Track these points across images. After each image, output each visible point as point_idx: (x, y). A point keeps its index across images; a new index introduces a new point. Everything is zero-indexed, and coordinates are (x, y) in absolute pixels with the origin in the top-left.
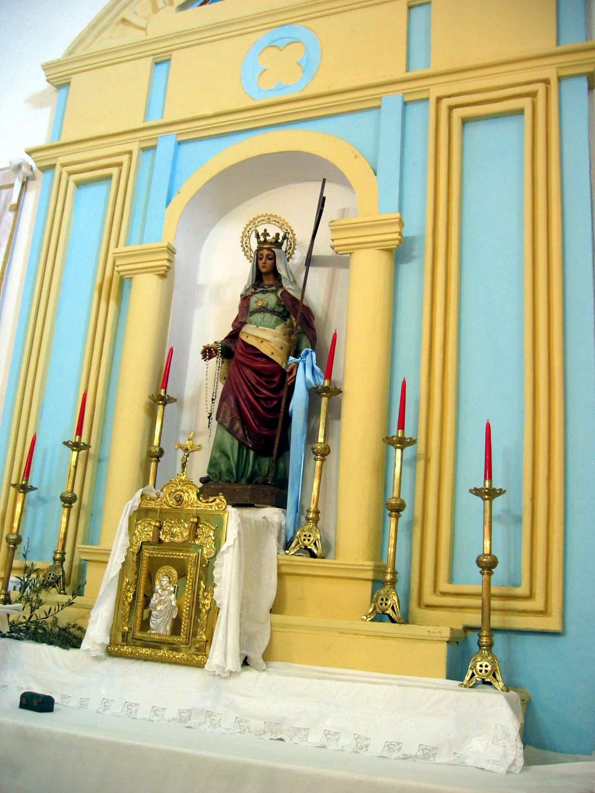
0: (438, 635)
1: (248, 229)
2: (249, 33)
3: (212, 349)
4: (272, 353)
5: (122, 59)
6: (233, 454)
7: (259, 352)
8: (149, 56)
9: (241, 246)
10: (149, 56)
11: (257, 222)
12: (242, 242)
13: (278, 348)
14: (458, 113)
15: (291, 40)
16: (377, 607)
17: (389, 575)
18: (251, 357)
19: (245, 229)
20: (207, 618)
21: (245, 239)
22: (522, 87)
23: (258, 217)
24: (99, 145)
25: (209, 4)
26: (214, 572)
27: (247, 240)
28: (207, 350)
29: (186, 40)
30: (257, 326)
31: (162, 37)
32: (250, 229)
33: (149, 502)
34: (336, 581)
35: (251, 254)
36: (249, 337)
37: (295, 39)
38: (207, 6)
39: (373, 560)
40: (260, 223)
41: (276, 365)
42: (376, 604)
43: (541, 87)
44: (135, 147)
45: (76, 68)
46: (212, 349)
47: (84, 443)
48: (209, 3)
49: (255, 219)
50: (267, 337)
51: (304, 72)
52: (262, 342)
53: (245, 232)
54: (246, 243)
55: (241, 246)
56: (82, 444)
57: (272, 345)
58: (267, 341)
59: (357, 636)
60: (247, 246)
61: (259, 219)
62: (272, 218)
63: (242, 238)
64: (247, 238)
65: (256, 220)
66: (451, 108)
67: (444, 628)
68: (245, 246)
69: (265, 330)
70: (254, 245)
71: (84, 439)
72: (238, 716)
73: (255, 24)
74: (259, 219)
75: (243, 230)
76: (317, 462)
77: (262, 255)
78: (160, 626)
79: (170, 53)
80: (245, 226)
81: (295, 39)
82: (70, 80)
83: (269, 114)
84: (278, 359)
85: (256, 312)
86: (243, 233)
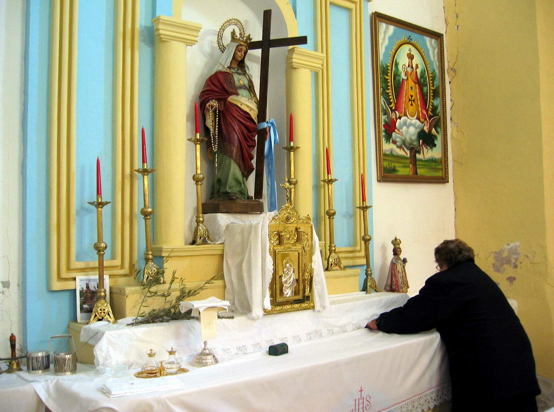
23: (233, 19)
49: (230, 20)
50: (246, 103)
77: (241, 49)
78: (288, 292)
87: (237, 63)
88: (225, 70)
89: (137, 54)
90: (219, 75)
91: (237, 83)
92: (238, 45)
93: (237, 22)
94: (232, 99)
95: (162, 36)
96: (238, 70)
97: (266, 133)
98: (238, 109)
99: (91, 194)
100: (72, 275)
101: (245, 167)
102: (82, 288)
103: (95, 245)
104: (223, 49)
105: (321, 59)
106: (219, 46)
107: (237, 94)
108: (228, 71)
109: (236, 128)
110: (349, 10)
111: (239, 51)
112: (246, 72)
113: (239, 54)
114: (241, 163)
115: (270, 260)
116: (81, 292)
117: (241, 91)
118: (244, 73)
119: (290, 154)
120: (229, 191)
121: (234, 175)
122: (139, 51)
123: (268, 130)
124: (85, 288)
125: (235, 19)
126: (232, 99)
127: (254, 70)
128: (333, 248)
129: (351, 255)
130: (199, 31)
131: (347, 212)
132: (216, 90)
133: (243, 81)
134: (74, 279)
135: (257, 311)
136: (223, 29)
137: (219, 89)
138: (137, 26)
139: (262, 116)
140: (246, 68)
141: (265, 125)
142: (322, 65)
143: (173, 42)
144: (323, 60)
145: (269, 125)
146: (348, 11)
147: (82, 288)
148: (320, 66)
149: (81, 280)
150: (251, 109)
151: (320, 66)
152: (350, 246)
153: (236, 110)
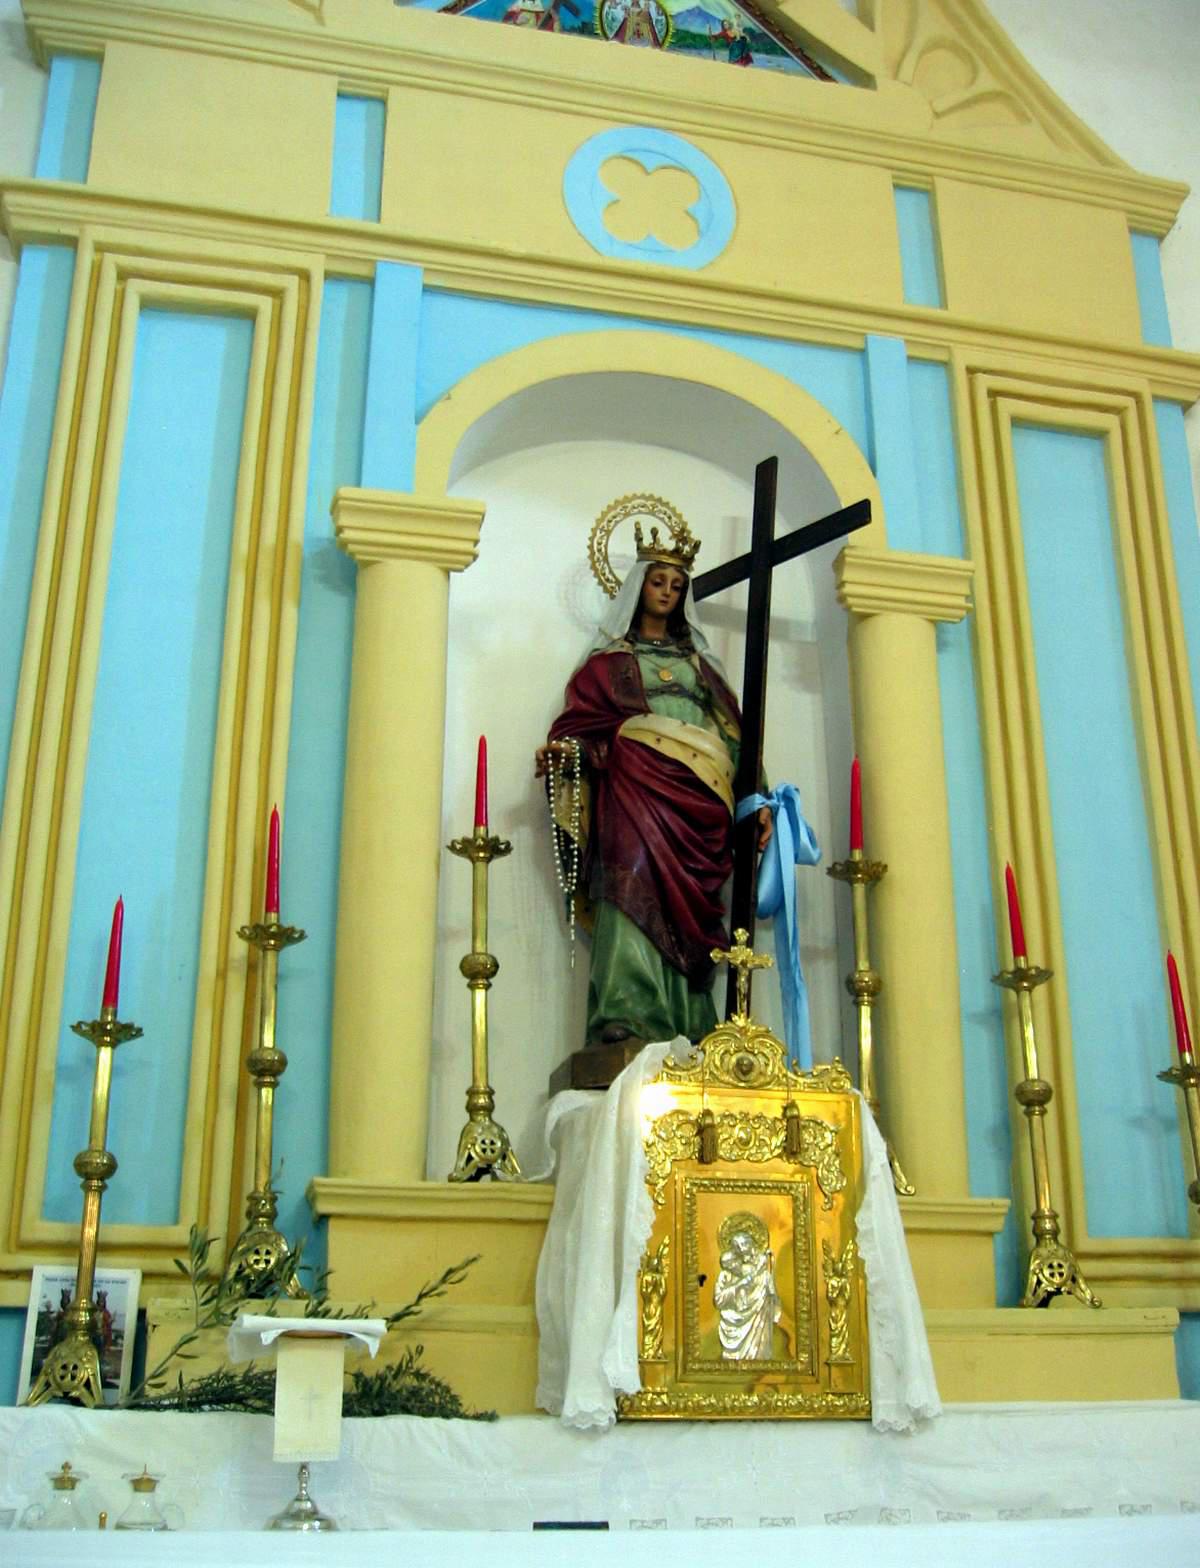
0: (1163, 1322)
1: (609, 516)
2: (539, 107)
3: (564, 755)
4: (716, 782)
5: (543, 102)
6: (658, 981)
7: (691, 775)
8: (333, 73)
9: (589, 547)
10: (333, 73)
11: (630, 505)
12: (591, 539)
13: (724, 775)
14: (136, 288)
15: (667, 162)
16: (1044, 1280)
17: (1047, 1221)
18: (675, 783)
19: (604, 514)
20: (662, 1312)
21: (598, 534)
22: (1075, 391)
23: (635, 497)
24: (214, 231)
25: (462, 15)
26: (856, 1219)
27: (602, 537)
28: (550, 755)
29: (929, 161)
30: (684, 723)
31: (231, 21)
32: (614, 517)
33: (672, 1072)
34: (378, 1225)
35: (603, 568)
36: (662, 742)
37: (676, 161)
38: (458, 19)
39: (1008, 1195)
40: (636, 510)
41: (722, 807)
42: (1041, 1276)
43: (292, 283)
44: (317, 266)
45: (297, 56)
46: (564, 755)
47: (1037, 968)
48: (463, 12)
49: (627, 499)
50: (693, 743)
51: (700, 233)
52: (695, 755)
53: (602, 520)
54: (599, 544)
55: (589, 547)
56: (1033, 972)
57: (714, 763)
58: (708, 756)
59: (1020, 1337)
60: (599, 550)
61: (636, 502)
62: (660, 507)
63: (594, 531)
64: (603, 533)
65: (630, 502)
66: (277, 294)
67: (1170, 1309)
68: (595, 549)
69: (700, 732)
70: (622, 547)
71: (1035, 958)
72: (940, 1509)
73: (677, 116)
74: (636, 502)
75: (599, 516)
76: (477, 991)
77: (663, 577)
78: (742, 1338)
79: (386, 86)
80: (605, 509)
81: (676, 161)
82: (1164, 231)
83: (463, 267)
84: (723, 791)
85: (663, 693)
86: (599, 521)
87: (663, 624)
88: (616, 649)
89: (290, 612)
90: (602, 672)
91: (649, 678)
92: (650, 568)
93: (656, 505)
94: (634, 728)
95: (351, 547)
96: (665, 643)
97: (762, 829)
98: (644, 753)
99: (92, 1011)
100: (21, 1261)
101: (679, 942)
102: (48, 1306)
103: (80, 1156)
104: (610, 587)
105: (960, 578)
106: (600, 583)
107: (645, 711)
108: (626, 647)
109: (647, 821)
110: (1100, 435)
111: (657, 585)
112: (692, 650)
113: (657, 593)
114: (658, 926)
115: (640, 1209)
116: (43, 1317)
117: (656, 702)
118: (687, 651)
119: (852, 891)
120: (612, 1014)
121: (626, 962)
122: (299, 603)
123: (763, 818)
124: (56, 1306)
125: (643, 497)
126: (634, 728)
127: (721, 643)
128: (1048, 1226)
129: (1170, 1268)
130: (479, 524)
131: (1152, 1111)
132: (598, 700)
133: (683, 672)
134: (27, 1274)
135: (586, 1399)
136: (604, 528)
137: (596, 705)
138: (296, 534)
139: (748, 772)
140: (694, 639)
141: (757, 801)
142: (970, 598)
143: (392, 562)
144: (971, 582)
145: (774, 801)
146: (1096, 443)
147: (48, 1306)
148: (961, 601)
149: (49, 1279)
150: (697, 753)
151: (961, 601)
152: (1174, 1234)
153: (641, 757)
